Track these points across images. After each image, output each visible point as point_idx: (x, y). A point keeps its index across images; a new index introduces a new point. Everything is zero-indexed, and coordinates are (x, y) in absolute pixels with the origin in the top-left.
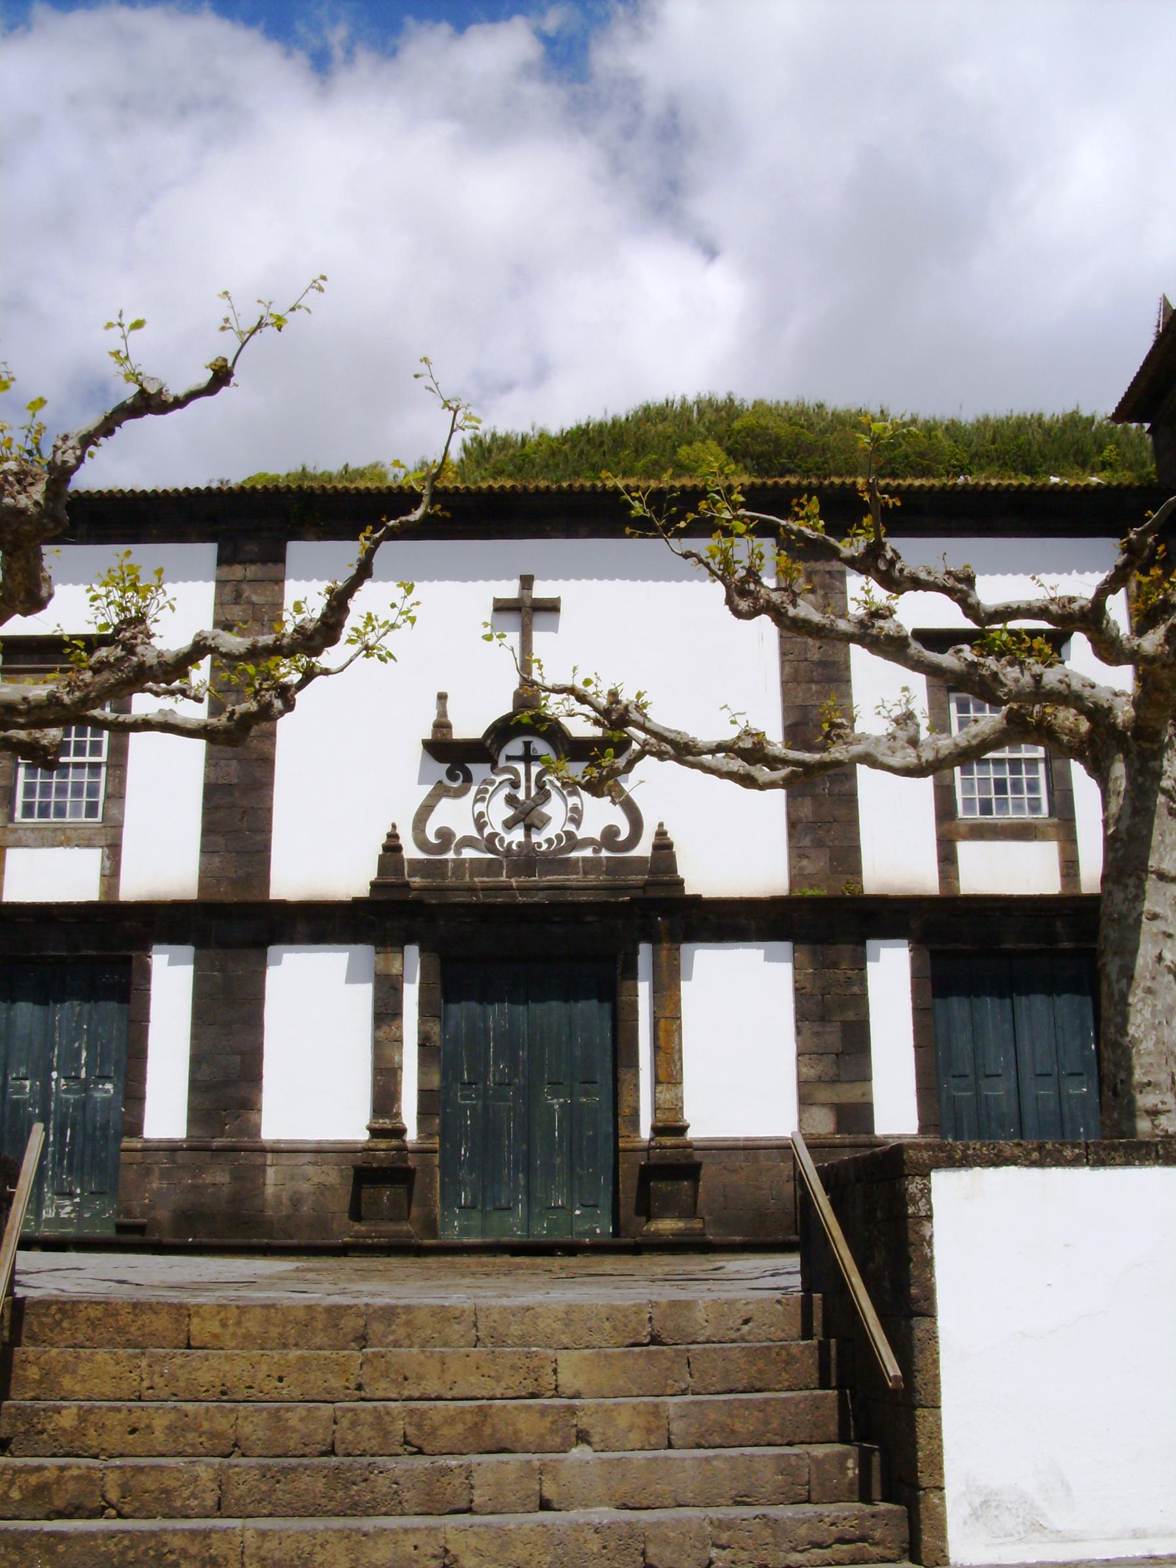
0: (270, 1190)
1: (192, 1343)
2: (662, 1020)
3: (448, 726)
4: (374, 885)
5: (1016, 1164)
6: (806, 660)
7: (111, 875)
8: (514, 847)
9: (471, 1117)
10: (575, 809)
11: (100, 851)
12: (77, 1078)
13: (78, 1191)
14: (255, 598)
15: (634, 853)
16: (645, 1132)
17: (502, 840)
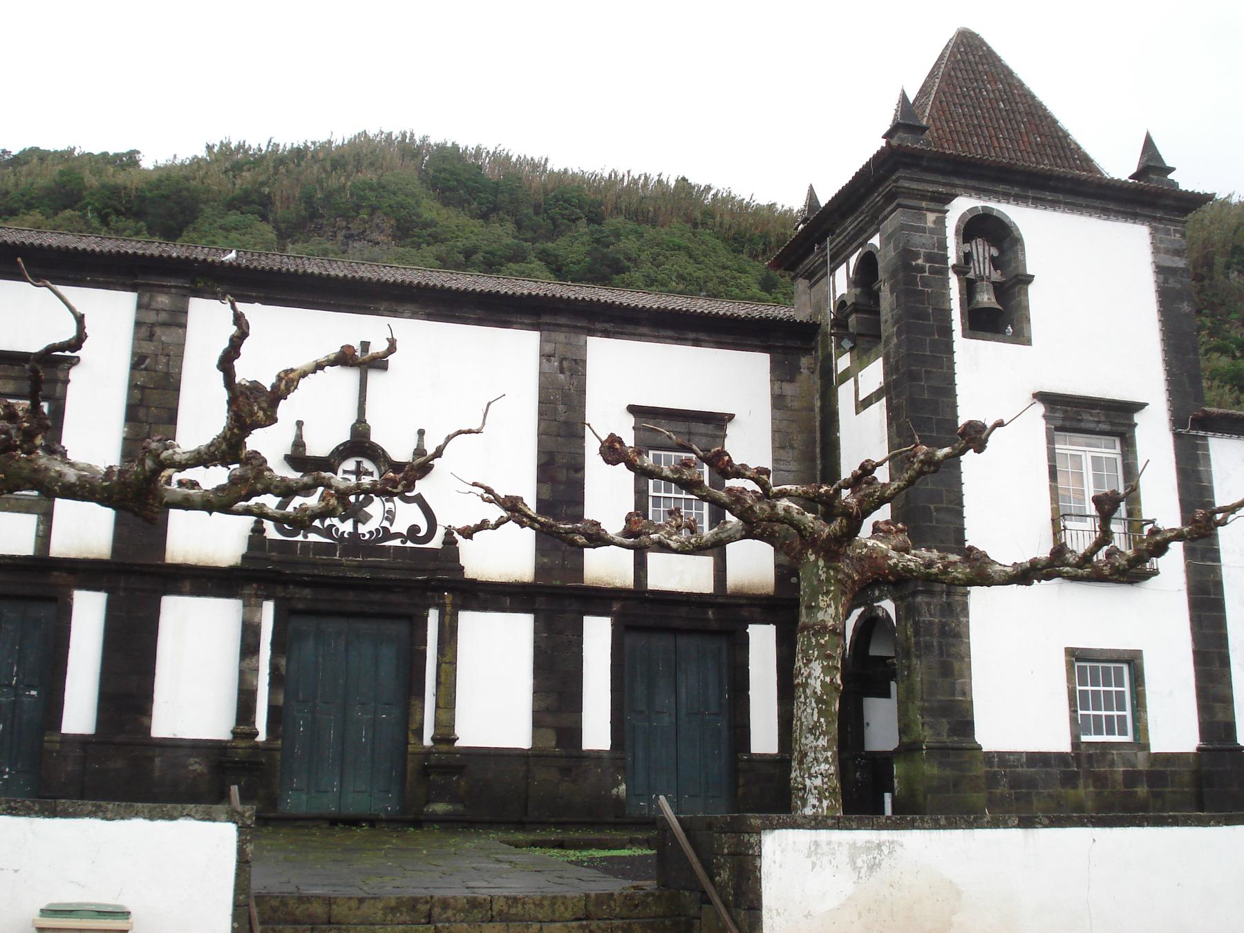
0: (157, 773)
1: (332, 920)
2: (443, 664)
3: (304, 445)
4: (244, 557)
5: (803, 828)
6: (555, 420)
7: (44, 538)
8: (346, 535)
9: (303, 726)
10: (389, 512)
11: (36, 516)
12: (9, 685)
13: (7, 770)
14: (163, 338)
15: (432, 545)
16: (427, 741)
17: (337, 530)
